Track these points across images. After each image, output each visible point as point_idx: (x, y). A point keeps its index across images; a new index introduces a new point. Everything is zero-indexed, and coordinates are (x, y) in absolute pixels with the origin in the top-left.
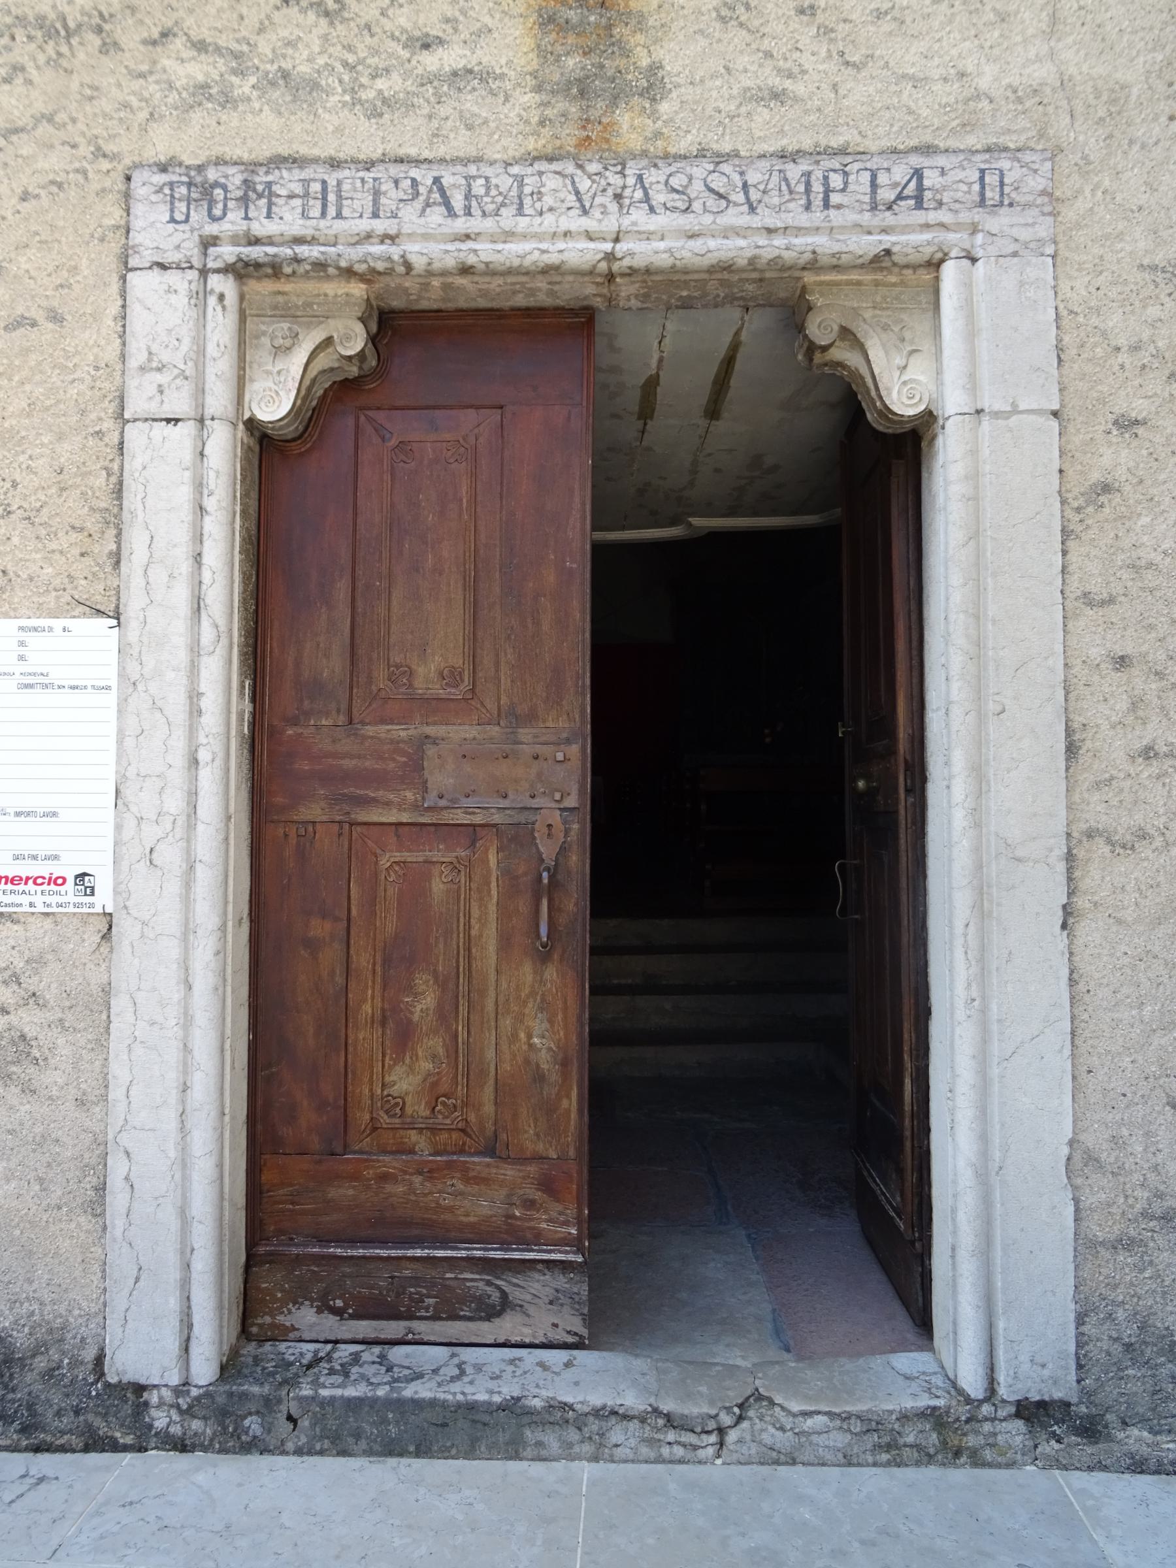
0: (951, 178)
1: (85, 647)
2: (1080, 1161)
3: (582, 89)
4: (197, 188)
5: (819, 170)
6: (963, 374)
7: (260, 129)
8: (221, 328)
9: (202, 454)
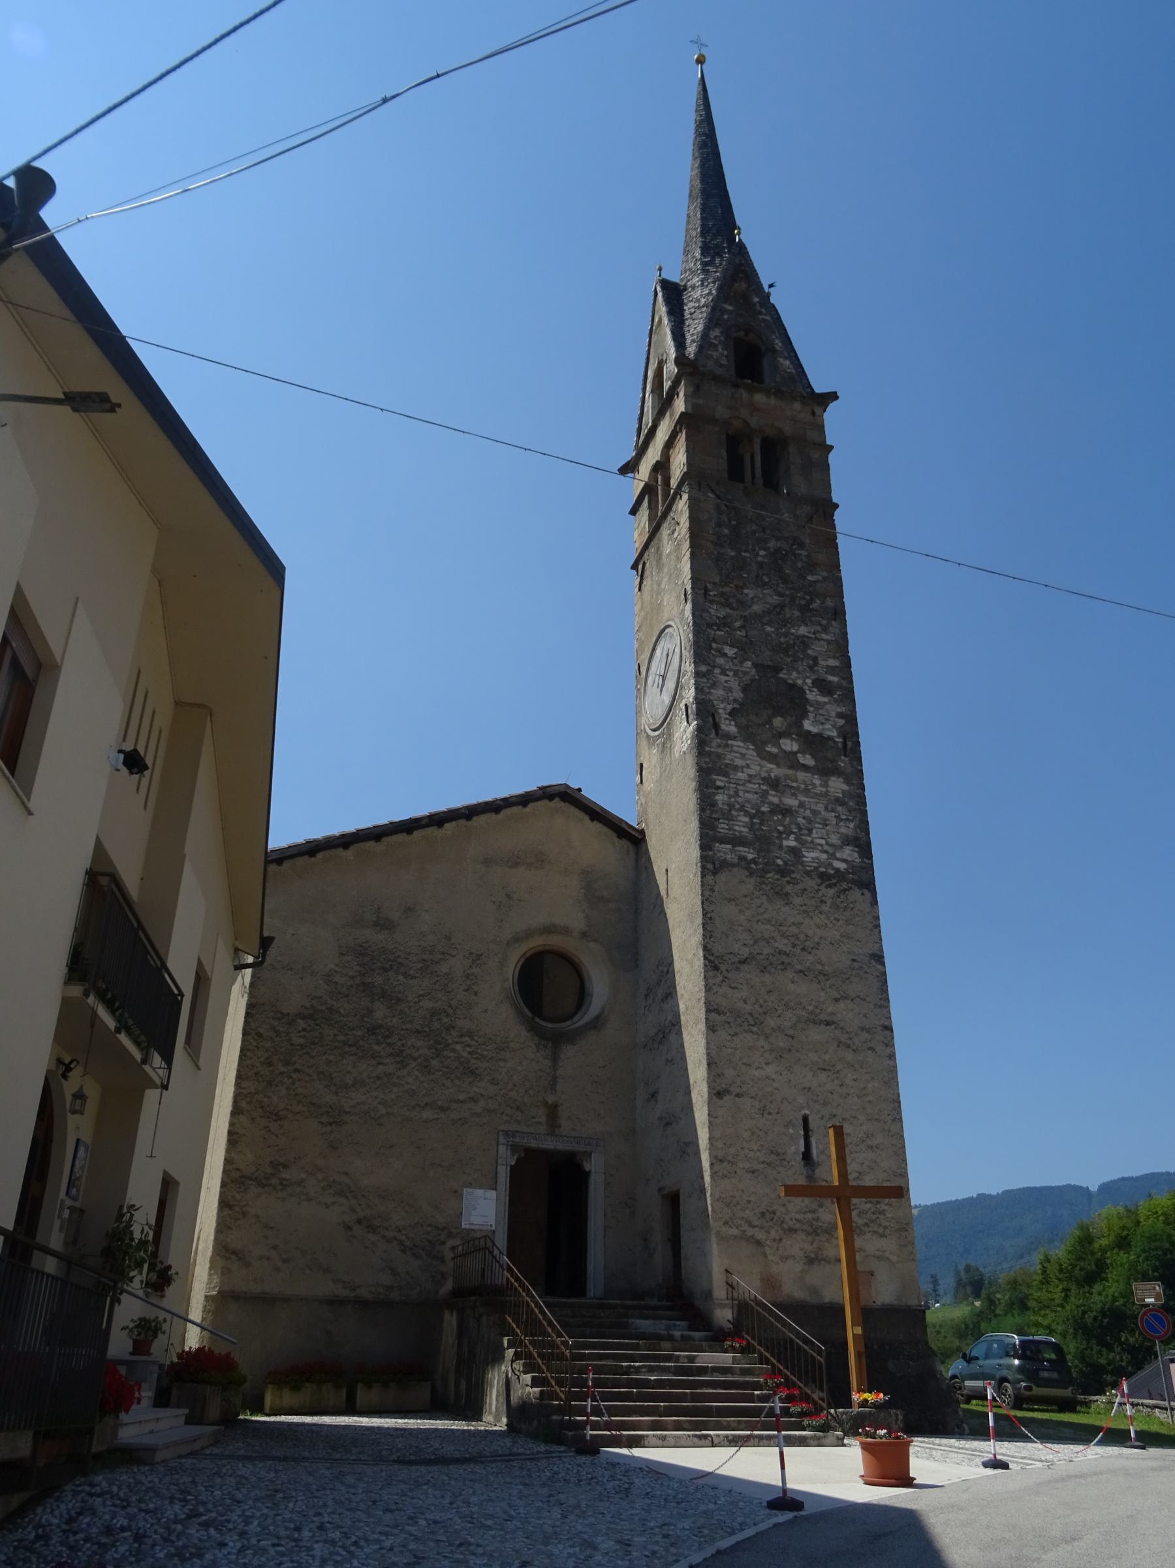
1: (492, 1194)
4: (507, 1133)
6: (595, 1166)
9: (516, 865)
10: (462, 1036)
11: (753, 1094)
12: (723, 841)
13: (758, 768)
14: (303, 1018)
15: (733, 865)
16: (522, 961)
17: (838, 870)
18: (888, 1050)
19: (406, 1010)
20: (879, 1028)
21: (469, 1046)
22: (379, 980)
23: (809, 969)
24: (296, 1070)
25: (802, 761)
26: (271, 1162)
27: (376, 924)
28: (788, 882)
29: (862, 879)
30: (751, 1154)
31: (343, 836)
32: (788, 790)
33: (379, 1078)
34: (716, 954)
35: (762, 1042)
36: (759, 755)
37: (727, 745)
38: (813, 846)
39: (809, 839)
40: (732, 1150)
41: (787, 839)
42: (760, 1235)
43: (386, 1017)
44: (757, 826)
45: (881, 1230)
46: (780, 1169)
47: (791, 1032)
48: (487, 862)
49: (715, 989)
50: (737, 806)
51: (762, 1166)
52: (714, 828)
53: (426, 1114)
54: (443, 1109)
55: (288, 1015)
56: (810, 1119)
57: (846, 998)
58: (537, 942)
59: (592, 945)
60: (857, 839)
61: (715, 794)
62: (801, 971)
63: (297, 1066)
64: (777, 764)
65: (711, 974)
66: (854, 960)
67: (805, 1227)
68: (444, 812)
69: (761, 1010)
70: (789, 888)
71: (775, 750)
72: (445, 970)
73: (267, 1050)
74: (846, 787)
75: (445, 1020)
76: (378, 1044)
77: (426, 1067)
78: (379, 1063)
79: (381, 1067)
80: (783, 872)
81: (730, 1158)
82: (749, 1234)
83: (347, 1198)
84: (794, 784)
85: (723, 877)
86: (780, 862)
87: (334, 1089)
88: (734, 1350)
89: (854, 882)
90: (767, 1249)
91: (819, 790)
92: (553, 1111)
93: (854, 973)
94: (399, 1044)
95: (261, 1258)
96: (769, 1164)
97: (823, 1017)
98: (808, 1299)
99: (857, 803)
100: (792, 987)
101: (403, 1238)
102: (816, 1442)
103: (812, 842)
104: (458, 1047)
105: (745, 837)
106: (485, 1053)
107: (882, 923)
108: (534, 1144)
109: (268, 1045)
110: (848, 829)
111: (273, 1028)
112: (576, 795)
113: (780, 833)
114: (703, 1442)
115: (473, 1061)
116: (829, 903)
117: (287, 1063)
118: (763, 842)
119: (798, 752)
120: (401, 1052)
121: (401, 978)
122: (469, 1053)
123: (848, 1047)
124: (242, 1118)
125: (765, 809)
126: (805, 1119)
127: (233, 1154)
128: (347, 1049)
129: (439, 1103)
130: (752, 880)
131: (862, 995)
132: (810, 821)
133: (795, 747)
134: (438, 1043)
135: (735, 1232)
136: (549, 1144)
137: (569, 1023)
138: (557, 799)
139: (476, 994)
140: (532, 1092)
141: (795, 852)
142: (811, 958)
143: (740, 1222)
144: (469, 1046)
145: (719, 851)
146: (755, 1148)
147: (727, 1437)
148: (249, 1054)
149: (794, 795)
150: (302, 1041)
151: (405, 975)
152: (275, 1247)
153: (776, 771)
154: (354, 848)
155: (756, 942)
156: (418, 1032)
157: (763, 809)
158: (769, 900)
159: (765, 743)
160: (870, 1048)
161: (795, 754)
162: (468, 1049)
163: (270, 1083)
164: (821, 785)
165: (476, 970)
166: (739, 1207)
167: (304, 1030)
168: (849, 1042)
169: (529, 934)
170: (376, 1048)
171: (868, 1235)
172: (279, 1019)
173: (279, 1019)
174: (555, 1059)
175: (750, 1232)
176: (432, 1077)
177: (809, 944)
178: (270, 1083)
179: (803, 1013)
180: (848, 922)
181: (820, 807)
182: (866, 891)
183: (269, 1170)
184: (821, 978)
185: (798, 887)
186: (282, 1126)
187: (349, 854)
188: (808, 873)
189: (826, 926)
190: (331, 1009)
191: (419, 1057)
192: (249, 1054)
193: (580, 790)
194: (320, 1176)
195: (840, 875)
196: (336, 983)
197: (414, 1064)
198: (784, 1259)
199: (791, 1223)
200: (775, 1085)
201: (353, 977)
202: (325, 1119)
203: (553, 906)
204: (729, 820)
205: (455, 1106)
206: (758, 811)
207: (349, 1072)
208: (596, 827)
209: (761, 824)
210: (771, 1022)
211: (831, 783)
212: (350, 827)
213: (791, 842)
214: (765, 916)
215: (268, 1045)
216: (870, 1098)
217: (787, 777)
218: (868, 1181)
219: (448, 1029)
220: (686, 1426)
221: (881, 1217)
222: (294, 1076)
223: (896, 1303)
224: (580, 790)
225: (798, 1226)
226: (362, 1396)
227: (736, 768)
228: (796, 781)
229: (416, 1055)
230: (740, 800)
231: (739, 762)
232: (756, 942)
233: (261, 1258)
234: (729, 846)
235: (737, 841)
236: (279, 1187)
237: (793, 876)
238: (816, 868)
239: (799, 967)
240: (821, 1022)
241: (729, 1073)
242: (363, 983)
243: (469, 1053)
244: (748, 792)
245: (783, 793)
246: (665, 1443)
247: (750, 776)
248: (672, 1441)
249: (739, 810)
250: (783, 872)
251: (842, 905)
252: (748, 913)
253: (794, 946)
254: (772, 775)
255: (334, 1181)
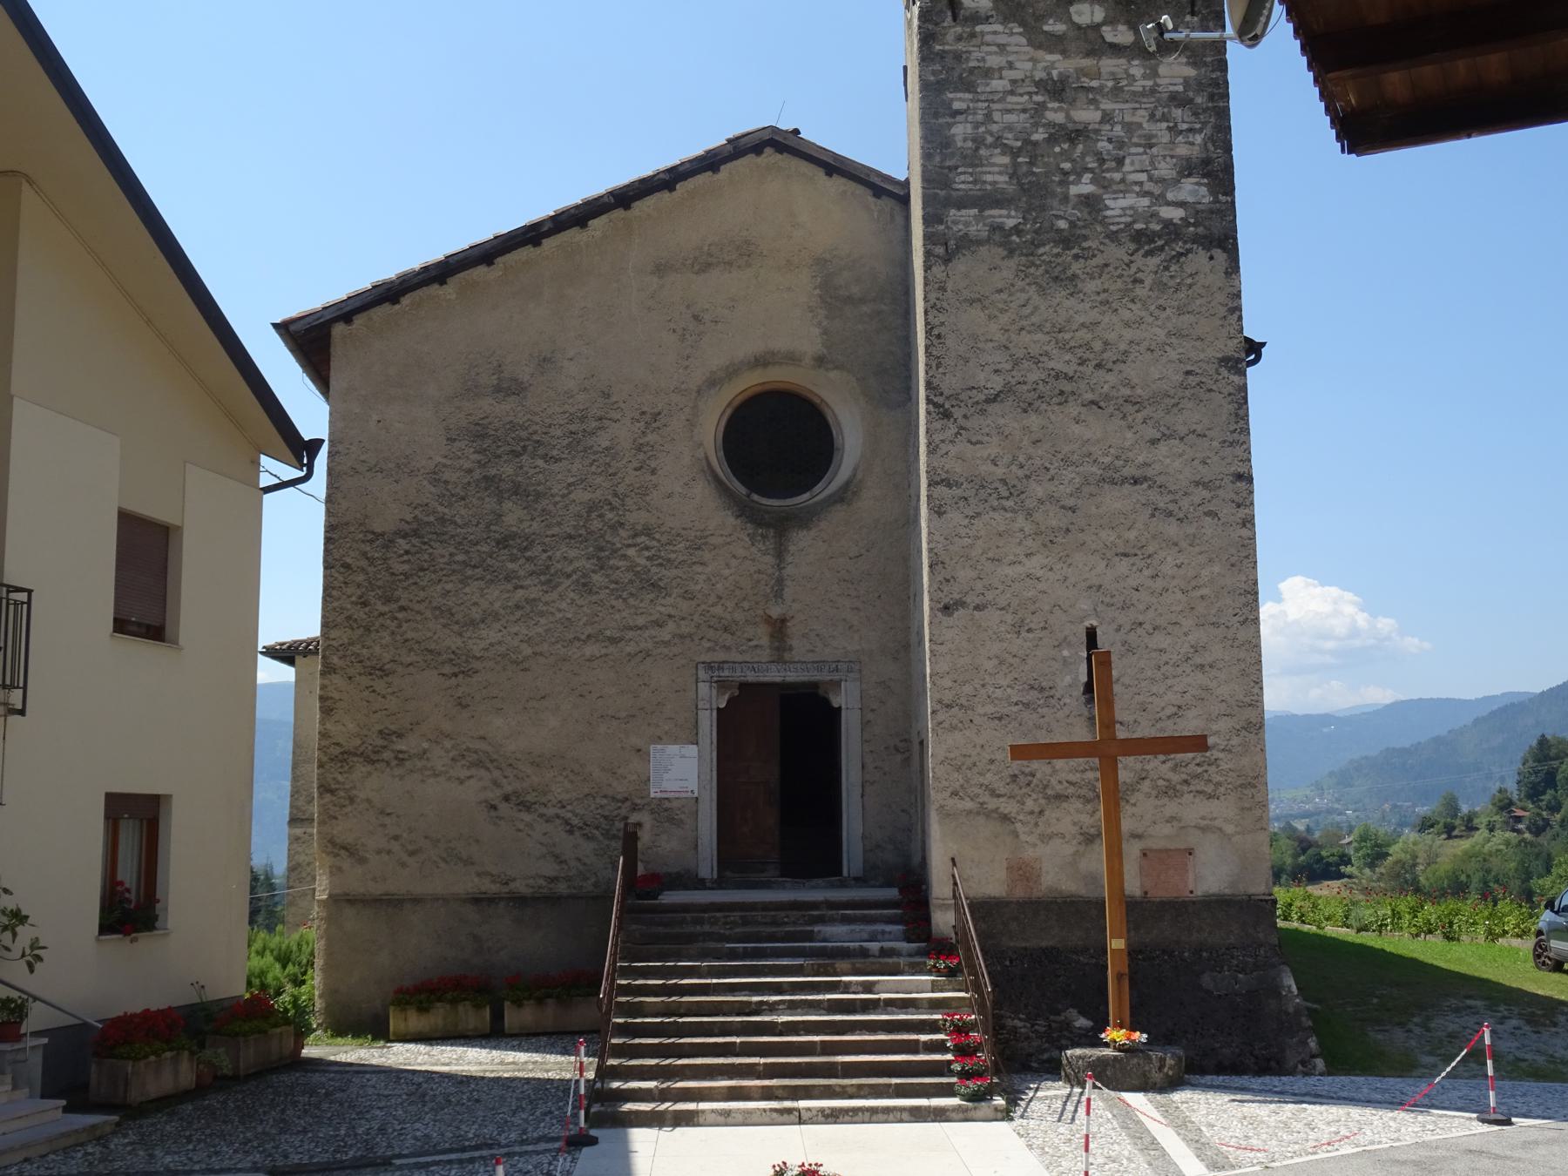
0: (843, 666)
1: (692, 750)
2: (864, 837)
3: (778, 649)
4: (709, 666)
5: (820, 664)
6: (846, 699)
7: (720, 656)
8: (714, 692)
9: (706, 267)
10: (635, 535)
11: (1003, 603)
12: (960, 205)
13: (1029, 65)
14: (404, 537)
15: (979, 243)
16: (729, 412)
17: (1168, 223)
18: (1242, 512)
19: (551, 507)
20: (1228, 480)
21: (647, 548)
22: (508, 470)
23: (1107, 397)
24: (402, 609)
25: (1109, 38)
26: (380, 732)
27: (498, 389)
28: (1076, 257)
29: (1217, 234)
30: (999, 693)
31: (425, 269)
32: (1082, 96)
33: (518, 607)
34: (947, 392)
35: (1021, 521)
36: (1030, 43)
37: (973, 35)
38: (1125, 187)
39: (1117, 176)
40: (968, 689)
41: (1078, 182)
42: (1008, 807)
43: (521, 521)
44: (1025, 169)
45: (1209, 789)
46: (1045, 710)
47: (1071, 502)
48: (660, 269)
49: (944, 448)
50: (990, 139)
51: (1015, 709)
52: (947, 184)
53: (590, 650)
54: (613, 640)
55: (383, 534)
56: (1099, 632)
57: (1170, 437)
58: (751, 381)
59: (833, 374)
60: (1206, 162)
61: (950, 126)
62: (1092, 402)
63: (402, 603)
64: (1064, 53)
65: (938, 425)
66: (1188, 373)
67: (1082, 792)
68: (577, 207)
69: (1020, 473)
70: (1076, 267)
71: (1060, 28)
72: (606, 444)
73: (359, 586)
74: (1191, 72)
75: (610, 515)
76: (514, 559)
77: (584, 585)
78: (516, 588)
79: (520, 592)
80: (1066, 241)
81: (963, 701)
82: (991, 806)
83: (488, 769)
84: (1095, 84)
85: (960, 265)
86: (1062, 224)
87: (456, 628)
88: (939, 972)
89: (1196, 239)
90: (1018, 825)
91: (1141, 84)
92: (779, 628)
93: (1187, 393)
94: (544, 556)
95: (379, 852)
96: (1027, 705)
97: (1128, 471)
98: (1083, 892)
99: (1211, 97)
100: (1077, 429)
101: (569, 815)
102: (961, 1116)
103: (1123, 181)
104: (631, 552)
105: (1003, 191)
106: (673, 556)
107: (1246, 302)
108: (751, 677)
109: (361, 578)
110: (1192, 147)
111: (364, 554)
112: (791, 142)
113: (1066, 173)
114: (786, 1117)
115: (654, 570)
116: (1148, 282)
117: (388, 600)
118: (1032, 193)
119: (1104, 23)
120: (548, 567)
121: (540, 462)
122: (648, 558)
123: (1170, 514)
124: (337, 680)
125: (1039, 136)
126: (1091, 635)
127: (328, 726)
128: (469, 572)
129: (608, 633)
130: (1012, 263)
131: (1199, 428)
132: (1120, 144)
133: (1099, 15)
134: (601, 549)
135: (969, 805)
136: (774, 675)
137: (806, 496)
138: (768, 150)
139: (653, 472)
140: (746, 605)
141: (1091, 203)
142: (1112, 378)
143: (977, 791)
144: (647, 548)
145: (955, 223)
146: (1004, 683)
147: (822, 1110)
148: (334, 593)
149: (1093, 102)
150: (406, 567)
151: (545, 457)
152: (396, 838)
153: (1058, 64)
154: (454, 282)
155: (1016, 364)
156: (570, 537)
157: (1036, 137)
158: (1042, 291)
159: (1041, 19)
160: (1210, 514)
161: (1096, 27)
162: (647, 554)
163: (368, 629)
164: (1144, 77)
165: (651, 438)
166: (975, 770)
167: (407, 552)
168: (1171, 507)
169: (732, 372)
170: (510, 566)
171: (1188, 798)
172: (371, 541)
173: (371, 541)
174: (780, 554)
175: (992, 803)
176: (594, 598)
177: (1109, 355)
178: (368, 629)
179: (1094, 469)
180: (1181, 311)
181: (1141, 116)
182: (1217, 253)
183: (380, 742)
184: (1129, 408)
185: (1094, 262)
186: (389, 684)
187: (449, 291)
188: (1113, 237)
189: (1141, 322)
190: (442, 520)
191: (574, 572)
192: (334, 593)
193: (796, 132)
194: (448, 744)
195: (1172, 231)
196: (446, 482)
197: (568, 582)
198: (1046, 838)
199: (1058, 787)
200: (1041, 586)
201: (470, 471)
202: (447, 669)
203: (772, 327)
204: (973, 165)
205: (630, 634)
206: (1027, 142)
207: (476, 604)
208: (838, 183)
209: (1031, 164)
210: (1038, 490)
211: (1162, 70)
212: (435, 254)
213: (1085, 187)
214: (1034, 319)
215: (361, 578)
216: (1204, 591)
217: (1081, 72)
218: (1145, 731)
219: (612, 527)
220: (779, 1093)
221: (1212, 769)
222: (400, 615)
223: (1227, 891)
224: (796, 132)
225: (1071, 790)
226: (513, 1017)
227: (988, 73)
228: (1098, 76)
229: (569, 569)
230: (995, 128)
231: (994, 61)
232: (1016, 364)
233: (379, 852)
234: (975, 211)
235: (988, 200)
236: (394, 763)
237: (1085, 245)
238: (1128, 225)
239: (1089, 396)
240: (1124, 480)
241: (964, 574)
242: (486, 478)
243: (648, 558)
244: (1009, 111)
245: (1073, 102)
246: (730, 1120)
247: (1013, 82)
248: (740, 1118)
249: (994, 146)
250: (1066, 241)
251: (1171, 283)
252: (1004, 319)
253: (1082, 362)
254: (1055, 73)
255: (468, 749)
